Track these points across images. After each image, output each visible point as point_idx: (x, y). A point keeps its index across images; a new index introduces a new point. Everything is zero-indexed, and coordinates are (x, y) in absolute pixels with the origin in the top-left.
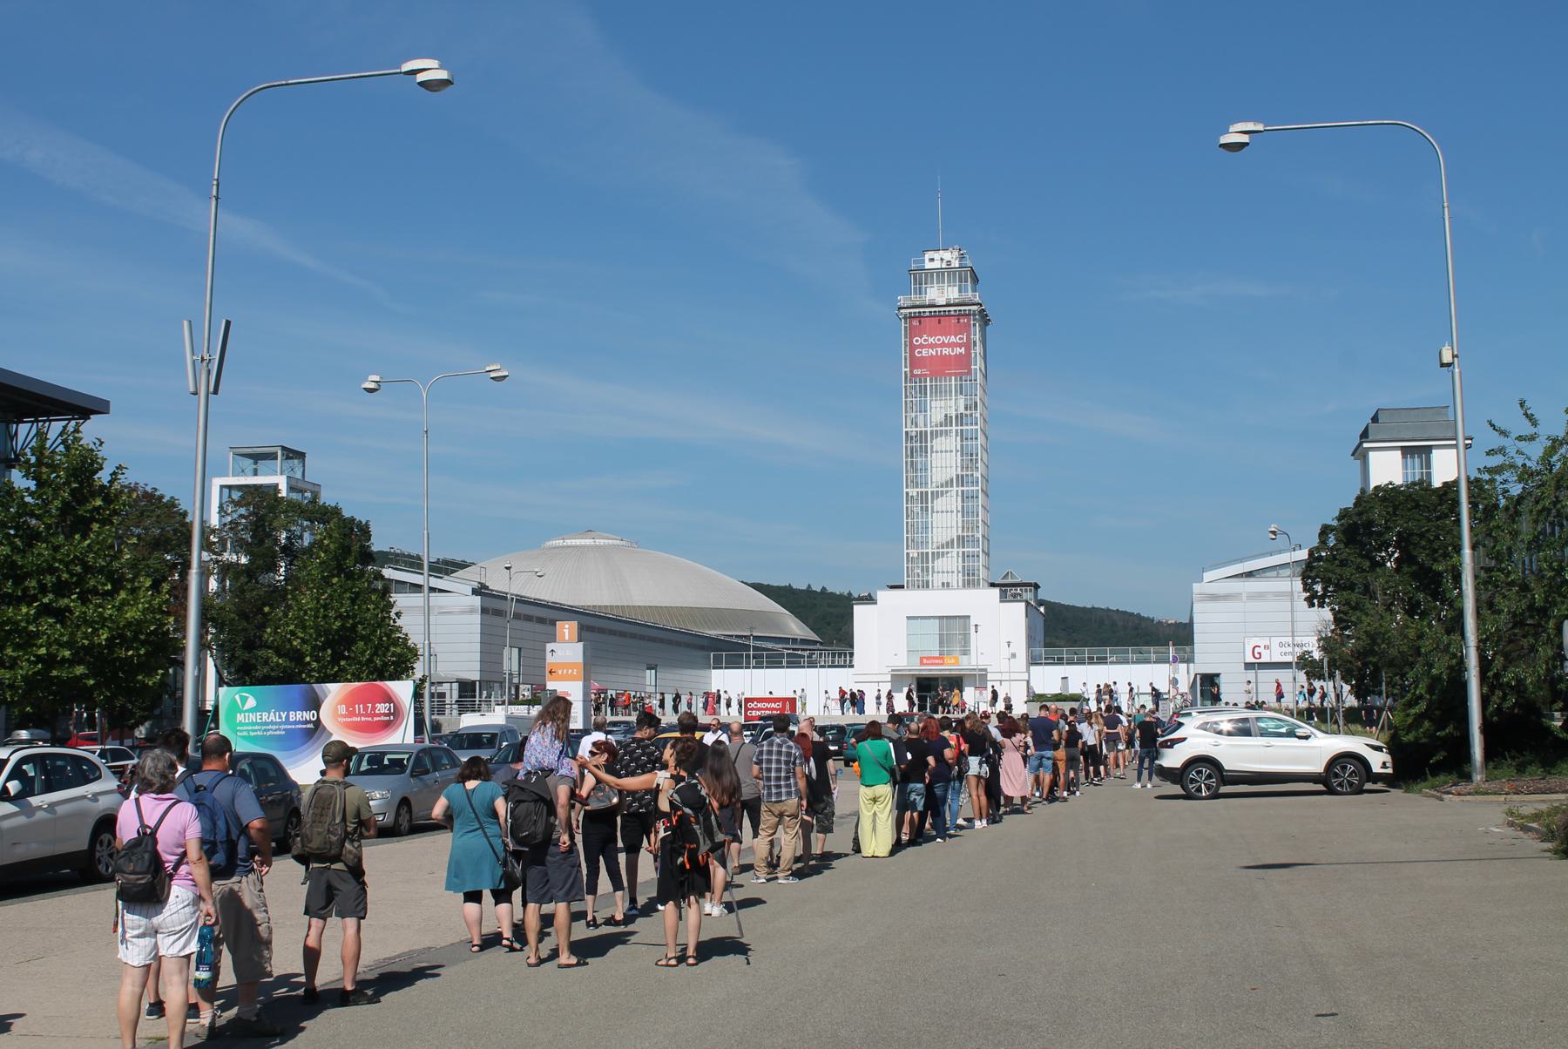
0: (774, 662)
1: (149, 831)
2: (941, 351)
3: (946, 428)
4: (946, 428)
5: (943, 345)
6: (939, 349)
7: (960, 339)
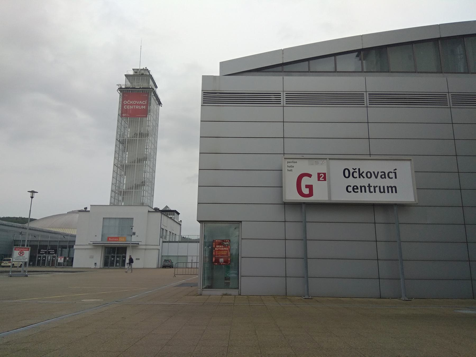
0: (110, 243)
1: (226, 284)
2: (135, 107)
3: (134, 139)
4: (134, 139)
5: (136, 104)
6: (134, 106)
7: (144, 102)
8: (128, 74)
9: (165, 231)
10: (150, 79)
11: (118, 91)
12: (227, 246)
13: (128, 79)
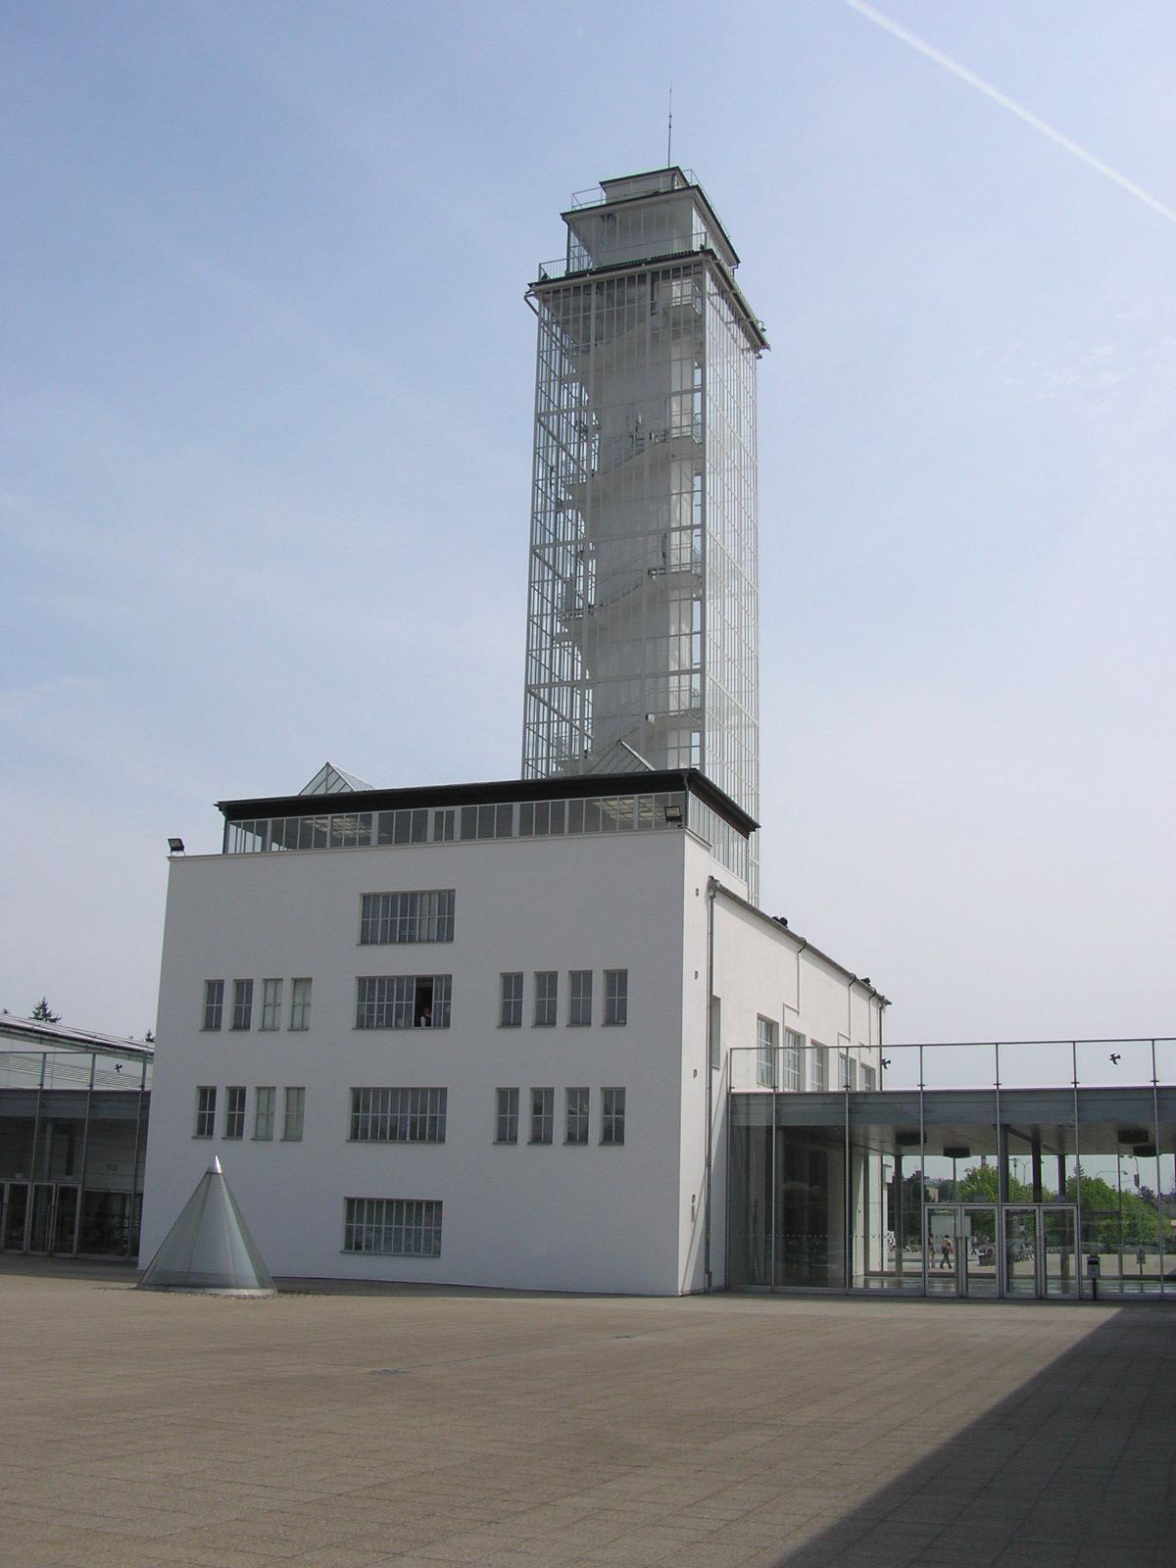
8: (579, 208)
9: (810, 1056)
10: (694, 211)
11: (532, 300)
12: (15, 1234)
13: (578, 235)
